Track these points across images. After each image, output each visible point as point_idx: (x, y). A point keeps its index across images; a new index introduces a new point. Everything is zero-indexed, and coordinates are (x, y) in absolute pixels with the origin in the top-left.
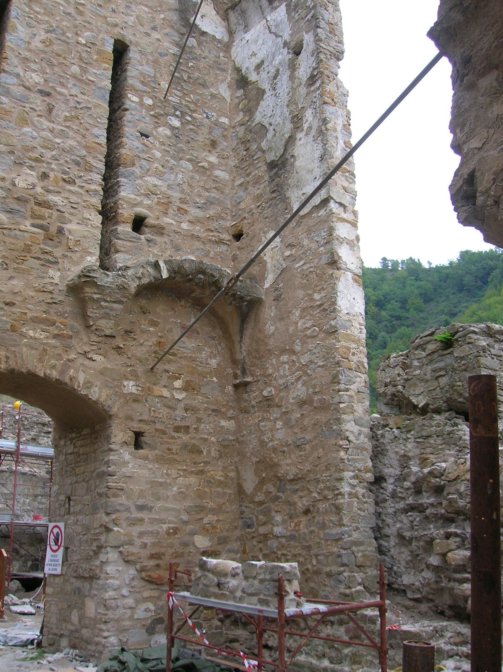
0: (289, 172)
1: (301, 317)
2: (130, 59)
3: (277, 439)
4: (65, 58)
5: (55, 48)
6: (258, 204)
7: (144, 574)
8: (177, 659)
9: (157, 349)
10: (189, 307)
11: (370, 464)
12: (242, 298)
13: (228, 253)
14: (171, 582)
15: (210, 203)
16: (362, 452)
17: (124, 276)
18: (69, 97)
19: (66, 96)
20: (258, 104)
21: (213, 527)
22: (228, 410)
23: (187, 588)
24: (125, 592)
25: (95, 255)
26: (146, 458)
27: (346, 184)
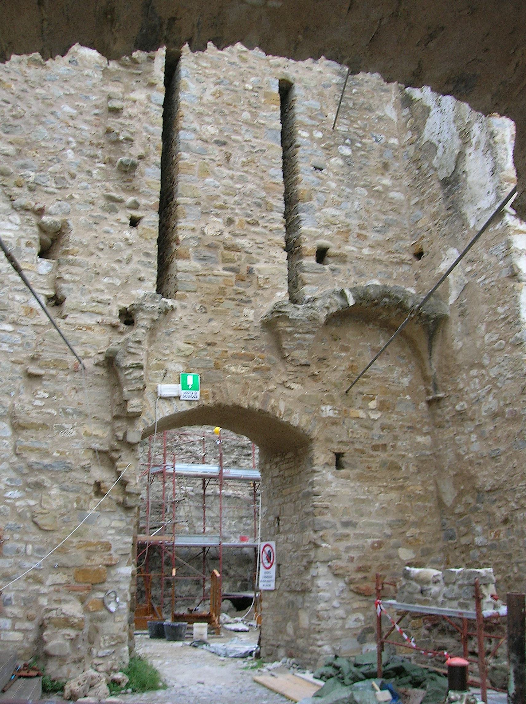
0: (463, 188)
1: (487, 331)
2: (296, 96)
3: (472, 452)
4: (235, 106)
5: (225, 98)
6: (436, 222)
7: (352, 587)
8: (387, 664)
9: (350, 372)
10: (378, 329)
12: (427, 316)
13: (411, 272)
14: (379, 591)
15: (388, 225)
17: (313, 308)
18: (244, 143)
20: (425, 122)
21: (416, 540)
22: (423, 426)
23: (394, 598)
24: (335, 603)
25: (284, 290)
26: (347, 477)
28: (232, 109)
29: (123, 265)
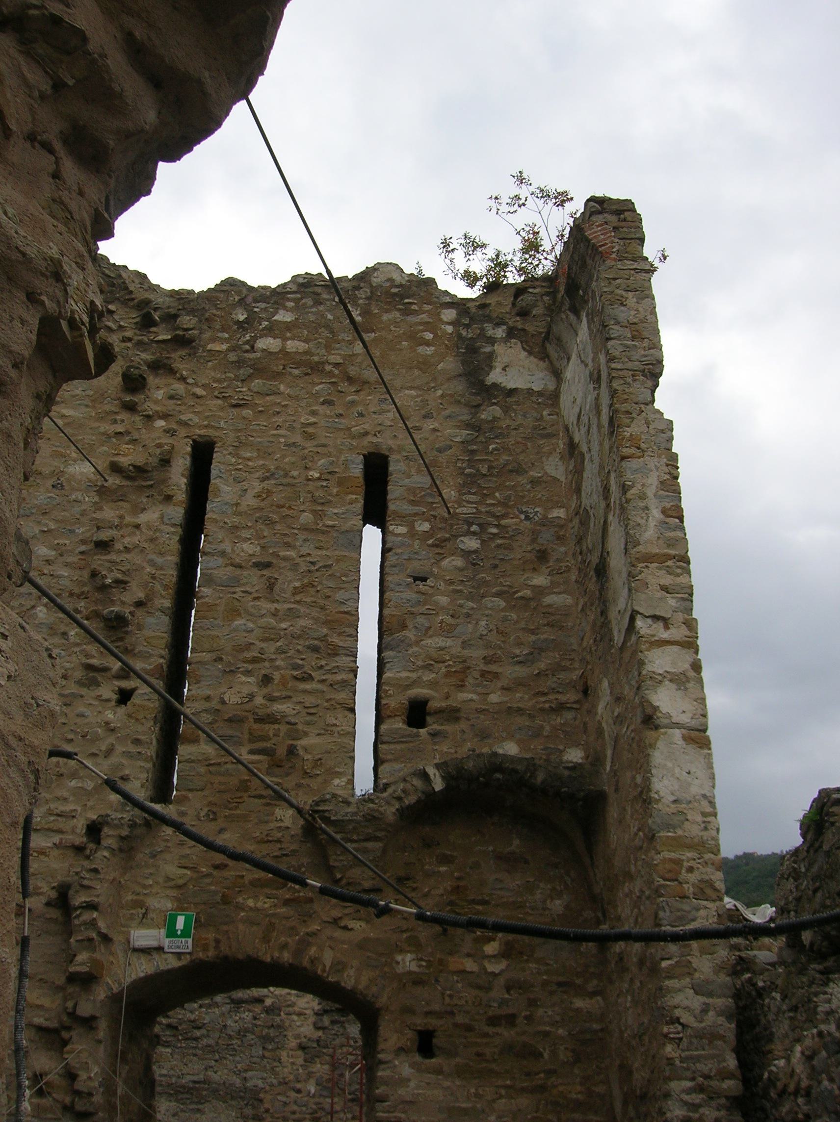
9: (453, 898)
11: (732, 1062)
13: (577, 722)
15: (538, 650)
16: (710, 1042)
18: (298, 560)
19: (293, 559)
26: (439, 1071)
27: (667, 580)
28: (285, 512)
29: (100, 760)
